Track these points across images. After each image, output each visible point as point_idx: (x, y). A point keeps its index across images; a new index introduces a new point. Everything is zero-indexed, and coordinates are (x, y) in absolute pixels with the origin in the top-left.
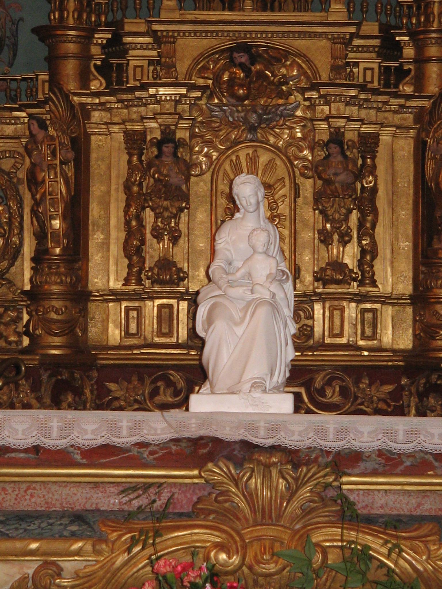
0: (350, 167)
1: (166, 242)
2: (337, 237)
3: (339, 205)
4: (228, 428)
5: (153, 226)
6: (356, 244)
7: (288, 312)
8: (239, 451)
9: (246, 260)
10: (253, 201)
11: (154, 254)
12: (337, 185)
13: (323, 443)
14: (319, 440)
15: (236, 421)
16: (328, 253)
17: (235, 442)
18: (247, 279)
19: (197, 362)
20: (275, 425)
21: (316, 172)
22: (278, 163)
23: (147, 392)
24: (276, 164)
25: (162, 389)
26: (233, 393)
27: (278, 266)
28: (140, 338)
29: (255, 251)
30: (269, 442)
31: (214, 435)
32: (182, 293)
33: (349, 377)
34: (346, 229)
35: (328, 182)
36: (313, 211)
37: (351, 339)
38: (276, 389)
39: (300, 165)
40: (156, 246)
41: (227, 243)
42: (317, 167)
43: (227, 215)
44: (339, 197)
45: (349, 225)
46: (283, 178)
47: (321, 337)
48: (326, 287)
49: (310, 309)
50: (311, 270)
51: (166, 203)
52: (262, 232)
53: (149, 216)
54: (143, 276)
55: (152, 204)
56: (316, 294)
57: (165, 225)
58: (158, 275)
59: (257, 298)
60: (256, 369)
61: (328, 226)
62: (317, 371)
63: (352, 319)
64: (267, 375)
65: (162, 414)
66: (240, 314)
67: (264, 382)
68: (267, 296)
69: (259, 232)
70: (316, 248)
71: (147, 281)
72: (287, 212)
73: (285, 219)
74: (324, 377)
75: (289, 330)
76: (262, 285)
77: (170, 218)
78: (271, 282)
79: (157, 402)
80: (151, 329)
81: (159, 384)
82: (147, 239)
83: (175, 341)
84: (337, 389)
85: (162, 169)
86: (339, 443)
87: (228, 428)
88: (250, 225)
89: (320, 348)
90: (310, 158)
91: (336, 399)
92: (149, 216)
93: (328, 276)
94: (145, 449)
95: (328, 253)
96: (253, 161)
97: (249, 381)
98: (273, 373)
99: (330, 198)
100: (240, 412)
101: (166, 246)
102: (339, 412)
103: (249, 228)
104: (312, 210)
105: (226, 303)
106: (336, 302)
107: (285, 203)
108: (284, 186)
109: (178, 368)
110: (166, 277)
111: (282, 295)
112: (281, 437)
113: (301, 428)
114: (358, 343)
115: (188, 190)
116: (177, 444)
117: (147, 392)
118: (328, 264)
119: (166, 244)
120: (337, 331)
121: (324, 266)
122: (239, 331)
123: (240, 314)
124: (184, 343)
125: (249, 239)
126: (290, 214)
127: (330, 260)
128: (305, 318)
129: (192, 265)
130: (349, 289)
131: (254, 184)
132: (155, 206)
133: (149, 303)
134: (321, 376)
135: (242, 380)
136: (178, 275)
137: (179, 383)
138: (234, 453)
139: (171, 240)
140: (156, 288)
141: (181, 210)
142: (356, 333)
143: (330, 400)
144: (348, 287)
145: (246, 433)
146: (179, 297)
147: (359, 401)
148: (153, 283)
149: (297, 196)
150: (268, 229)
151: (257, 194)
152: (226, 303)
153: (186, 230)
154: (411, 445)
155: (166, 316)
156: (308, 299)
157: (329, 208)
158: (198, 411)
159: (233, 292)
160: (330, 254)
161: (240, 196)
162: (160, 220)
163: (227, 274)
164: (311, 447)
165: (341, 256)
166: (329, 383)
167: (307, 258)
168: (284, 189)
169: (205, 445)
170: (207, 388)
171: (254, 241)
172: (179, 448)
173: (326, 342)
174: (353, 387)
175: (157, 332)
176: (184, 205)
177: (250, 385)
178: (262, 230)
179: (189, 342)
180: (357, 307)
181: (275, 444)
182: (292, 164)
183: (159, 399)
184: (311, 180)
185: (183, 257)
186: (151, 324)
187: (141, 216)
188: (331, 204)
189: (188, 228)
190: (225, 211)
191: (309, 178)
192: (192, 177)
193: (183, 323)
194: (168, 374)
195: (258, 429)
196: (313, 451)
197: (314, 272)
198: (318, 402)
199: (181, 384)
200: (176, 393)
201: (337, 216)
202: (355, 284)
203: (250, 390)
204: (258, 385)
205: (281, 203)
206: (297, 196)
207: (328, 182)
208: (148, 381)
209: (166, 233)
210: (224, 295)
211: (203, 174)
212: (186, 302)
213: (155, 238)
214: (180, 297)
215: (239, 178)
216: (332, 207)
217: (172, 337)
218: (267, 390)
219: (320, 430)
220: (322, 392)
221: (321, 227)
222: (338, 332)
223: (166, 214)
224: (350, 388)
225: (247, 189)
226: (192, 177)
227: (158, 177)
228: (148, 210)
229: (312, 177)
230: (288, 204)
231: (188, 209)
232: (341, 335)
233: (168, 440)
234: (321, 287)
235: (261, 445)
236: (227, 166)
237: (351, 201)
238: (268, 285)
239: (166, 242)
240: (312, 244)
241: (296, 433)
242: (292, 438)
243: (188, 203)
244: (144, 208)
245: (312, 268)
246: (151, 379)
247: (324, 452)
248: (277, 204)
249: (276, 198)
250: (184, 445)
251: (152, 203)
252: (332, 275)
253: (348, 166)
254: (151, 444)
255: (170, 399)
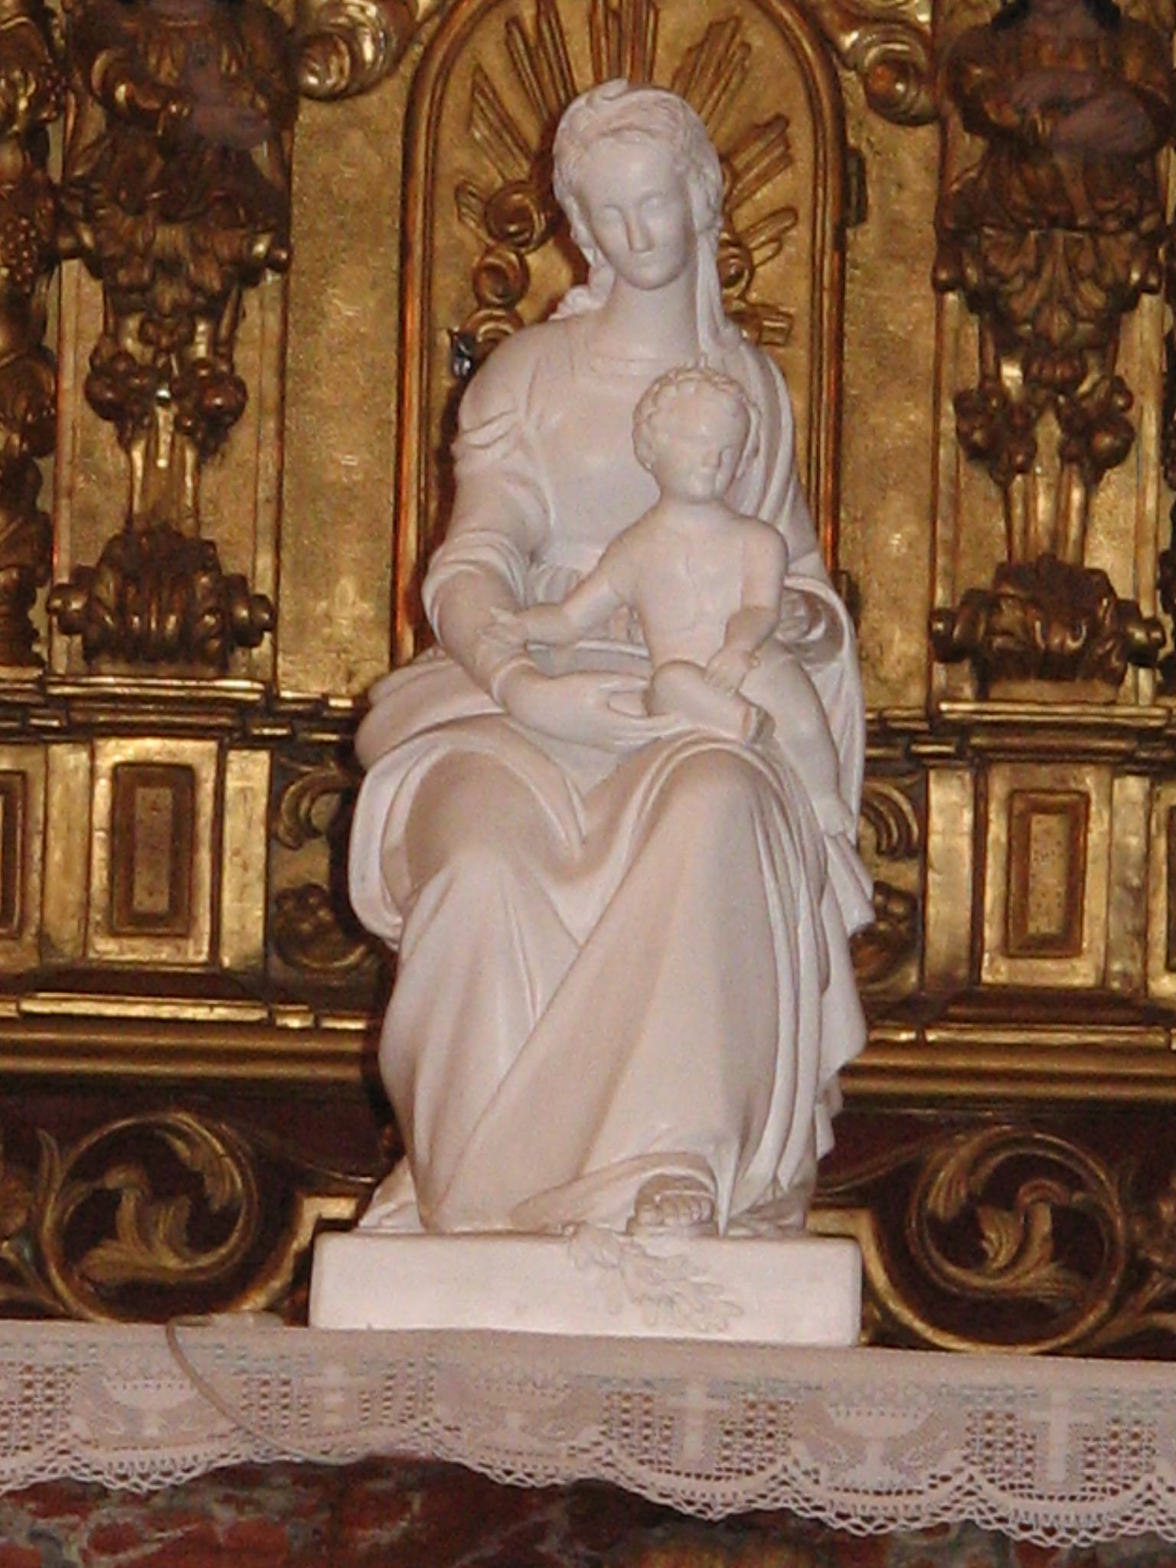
0: (1133, 67)
1: (165, 438)
2: (1058, 432)
3: (1072, 265)
4: (514, 1420)
5: (96, 351)
6: (1152, 473)
7: (832, 813)
8: (569, 1538)
9: (621, 537)
10: (661, 225)
11: (98, 498)
12: (1061, 161)
13: (1010, 1504)
14: (990, 1491)
15: (561, 1381)
16: (1008, 518)
17: (551, 1493)
18: (623, 635)
19: (352, 1073)
20: (766, 1404)
21: (955, 90)
22: (757, 42)
23: (49, 1221)
24: (746, 46)
25: (128, 1206)
26: (540, 1233)
27: (786, 572)
28: (16, 936)
29: (666, 492)
30: (729, 1496)
31: (441, 1453)
32: (242, 708)
33: (1110, 1161)
34: (1101, 393)
35: (1012, 146)
36: (931, 294)
37: (1116, 967)
38: (766, 1219)
39: (873, 53)
40: (110, 457)
41: (521, 443)
42: (957, 69)
43: (483, 303)
44: (1071, 227)
45: (1119, 370)
46: (781, 121)
47: (964, 953)
48: (996, 692)
49: (906, 807)
50: (916, 607)
51: (169, 237)
52: (708, 390)
53: (76, 299)
54: (37, 615)
55: (99, 244)
56: (937, 726)
57: (159, 351)
58: (121, 611)
59: (679, 736)
60: (667, 1110)
61: (1011, 372)
62: (943, 1131)
63: (1125, 861)
64: (719, 1141)
65: (170, 1334)
66: (582, 817)
67: (705, 1180)
68: (729, 727)
69: (691, 388)
70: (943, 485)
71: (60, 642)
72: (796, 299)
73: (787, 333)
74: (977, 1162)
75: (838, 907)
76: (702, 671)
77: (188, 314)
78: (750, 656)
79: (99, 1275)
80: (74, 895)
81: (115, 1179)
82: (66, 422)
83: (203, 958)
84: (1044, 1224)
85: (153, 61)
86: (1094, 1508)
87: (514, 1420)
88: (641, 350)
89: (953, 1010)
90: (924, 18)
91: (1038, 1276)
92: (76, 299)
93: (1006, 633)
94: (74, 1519)
95: (1008, 518)
96: (628, 26)
97: (630, 1174)
98: (753, 1137)
99: (1023, 230)
100: (579, 1332)
101: (162, 463)
102: (1046, 1346)
103: (636, 370)
104: (926, 289)
105: (516, 760)
106: (1045, 769)
107: (790, 249)
108: (787, 160)
109: (214, 1099)
110: (161, 622)
111: (807, 726)
112: (794, 1471)
113: (904, 1426)
114: (1153, 986)
115: (286, 169)
116: (242, 1494)
117: (49, 1221)
118: (1005, 573)
119: (163, 449)
120: (1043, 924)
121: (984, 580)
122: (578, 907)
123: (582, 817)
124: (248, 971)
125: (637, 426)
126: (815, 305)
127: (1018, 553)
128: (879, 852)
129: (296, 563)
130: (1112, 703)
131: (672, 139)
132: (111, 250)
133: (70, 758)
134: (965, 1152)
135: (591, 1167)
136: (225, 613)
137: (220, 1175)
138: (543, 1549)
139: (190, 433)
140: (110, 681)
141: (248, 274)
142: (1142, 935)
143: (1004, 1282)
144: (1105, 692)
145: (614, 1445)
146: (230, 730)
147: (1155, 1289)
148: (90, 653)
149: (852, 214)
150: (735, 374)
151: (680, 191)
152: (516, 760)
153: (270, 381)
154: (1109, 1507)
155: (158, 828)
156: (897, 753)
157: (1018, 282)
158: (363, 1326)
159: (549, 703)
160: (1018, 525)
161: (597, 198)
162: (133, 323)
163: (519, 608)
164: (945, 1527)
165: (1074, 532)
166: (1000, 1192)
167: (896, 539)
168: (788, 174)
169: (390, 1507)
170: (402, 1207)
171: (663, 438)
172: (249, 1516)
173: (986, 977)
174: (1128, 1216)
175: (108, 913)
176: (261, 248)
177: (630, 1193)
178: (708, 379)
179: (275, 961)
180: (1151, 797)
181: (761, 1504)
182: (826, 43)
183: (114, 1258)
184: (926, 136)
185: (248, 522)
186: (79, 870)
187: (34, 303)
188: (1030, 262)
189: (282, 373)
190: (476, 283)
191: (916, 121)
192: (305, 103)
193: (245, 867)
194: (169, 1128)
195: (671, 1425)
196: (959, 1544)
197: (934, 614)
198: (934, 1287)
199: (231, 1183)
200: (205, 1229)
201: (1058, 324)
202: (1146, 679)
203: (632, 1221)
204: (671, 1195)
205: (767, 251)
206: (852, 214)
207: (1012, 146)
208: (56, 1164)
209: (164, 393)
210: (503, 720)
211: (363, 90)
212: (263, 756)
213: (107, 418)
214: (235, 727)
215: (589, 102)
216: (1034, 275)
217: (185, 936)
218: (722, 1224)
219: (1000, 1437)
220: (962, 1238)
221: (971, 378)
222: (1053, 929)
223: (168, 295)
224: (1111, 1224)
225: (631, 160)
226: (305, 103)
227: (129, 98)
228: (72, 268)
229: (935, 117)
230: (805, 256)
231: (282, 268)
232: (1064, 942)
233: (195, 1474)
234: (968, 691)
235: (689, 1510)
236: (489, 51)
237: (1134, 248)
238: (732, 667)
239: (165, 438)
240: (925, 469)
241: (874, 1452)
242: (849, 1478)
243: (282, 240)
244: (50, 261)
245: (922, 591)
246: (74, 1154)
247: (1012, 1552)
248: (748, 254)
249: (741, 225)
250: (276, 1499)
251: (95, 232)
252: (1028, 630)
253: (1118, 62)
254: (104, 1492)
255: (172, 1262)
